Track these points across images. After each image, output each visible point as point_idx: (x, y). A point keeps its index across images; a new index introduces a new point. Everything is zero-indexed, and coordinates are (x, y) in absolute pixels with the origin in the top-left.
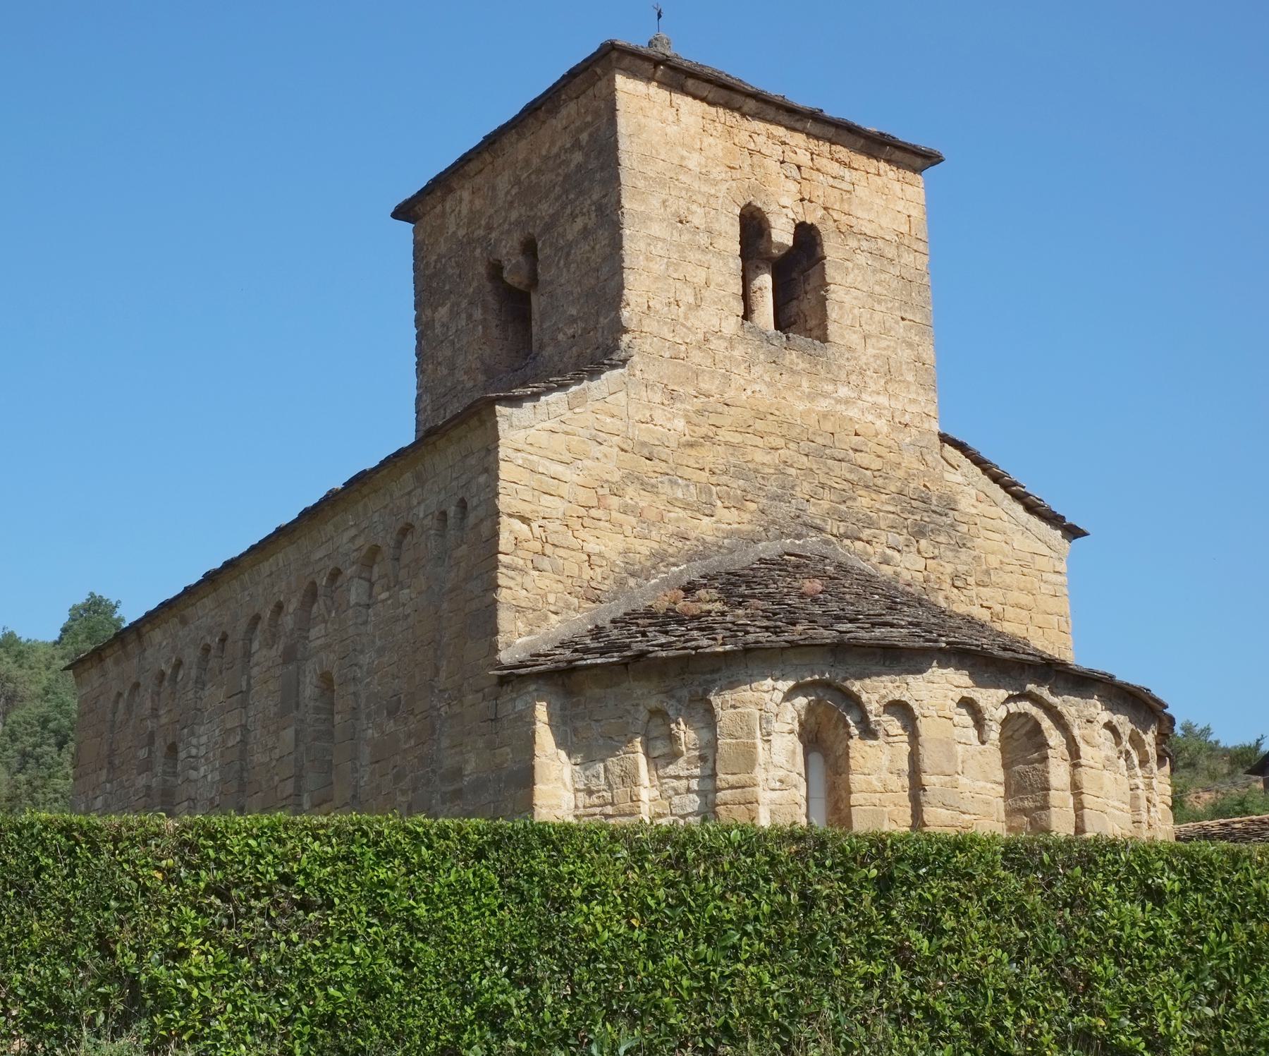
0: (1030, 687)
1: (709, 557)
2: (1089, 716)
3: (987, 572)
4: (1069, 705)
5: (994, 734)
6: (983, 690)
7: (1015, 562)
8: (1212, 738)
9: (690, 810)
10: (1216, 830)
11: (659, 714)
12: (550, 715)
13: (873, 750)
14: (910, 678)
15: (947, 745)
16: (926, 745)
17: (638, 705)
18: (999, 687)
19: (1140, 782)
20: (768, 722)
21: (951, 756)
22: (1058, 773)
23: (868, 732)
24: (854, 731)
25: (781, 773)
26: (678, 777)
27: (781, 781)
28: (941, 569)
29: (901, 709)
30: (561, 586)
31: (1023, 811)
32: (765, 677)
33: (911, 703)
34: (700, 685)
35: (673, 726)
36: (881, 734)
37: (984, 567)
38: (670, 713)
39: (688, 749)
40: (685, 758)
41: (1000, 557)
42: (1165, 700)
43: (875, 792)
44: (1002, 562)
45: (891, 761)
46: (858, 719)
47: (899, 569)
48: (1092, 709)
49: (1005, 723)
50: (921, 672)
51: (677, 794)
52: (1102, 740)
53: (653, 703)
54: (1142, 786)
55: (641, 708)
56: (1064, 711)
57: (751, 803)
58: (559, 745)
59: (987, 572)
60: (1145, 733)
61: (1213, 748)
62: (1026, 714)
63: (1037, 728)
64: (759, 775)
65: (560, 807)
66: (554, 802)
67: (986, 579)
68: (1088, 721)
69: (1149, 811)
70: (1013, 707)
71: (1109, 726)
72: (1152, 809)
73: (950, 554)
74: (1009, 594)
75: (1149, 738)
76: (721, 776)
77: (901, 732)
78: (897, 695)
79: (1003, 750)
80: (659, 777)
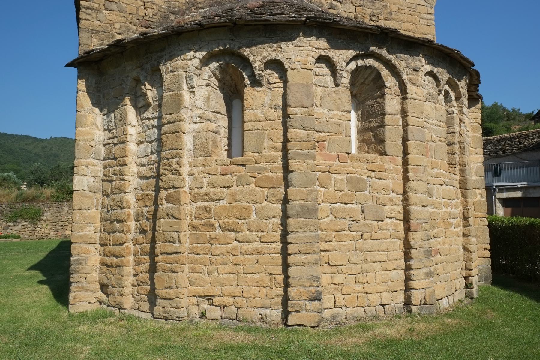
0: (373, 48)
1: (224, 4)
2: (417, 71)
3: (391, 13)
4: (400, 61)
5: (346, 79)
6: (337, 51)
7: (407, 9)
8: (520, 112)
9: (153, 138)
10: (517, 135)
11: (138, 82)
12: (88, 87)
13: (259, 94)
14: (283, 45)
15: (307, 87)
16: (291, 88)
17: (128, 77)
18: (349, 49)
19: (455, 110)
20: (191, 79)
21: (310, 95)
22: (392, 103)
23: (256, 83)
24: (248, 82)
25: (200, 112)
26: (149, 119)
27: (200, 117)
28: (364, 12)
29: (276, 65)
30: (124, 19)
31: (370, 129)
32: (190, 51)
33: (283, 61)
34: (155, 60)
35: (143, 87)
36: (264, 83)
37: (389, 11)
38: (141, 79)
39: (154, 101)
40: (152, 107)
41: (399, 6)
42: (472, 59)
43: (260, 121)
44: (399, 9)
45: (271, 100)
46: (250, 74)
47: (340, 11)
48: (418, 62)
49: (355, 73)
50: (291, 40)
51: (149, 129)
52: (426, 83)
53: (134, 74)
54: (456, 112)
55: (129, 78)
56: (397, 63)
57: (178, 132)
58: (95, 104)
59: (391, 13)
60: (459, 81)
61: (520, 115)
62: (370, 67)
63: (378, 76)
64: (185, 114)
65: (93, 140)
66: (89, 137)
67: (389, 17)
68: (414, 70)
69: (460, 126)
70: (360, 62)
71: (430, 74)
72: (462, 125)
73: (369, 4)
74: (402, 25)
75: (463, 84)
76: (164, 116)
77: (278, 80)
78: (274, 56)
79: (88, 93)
80: (142, 120)
